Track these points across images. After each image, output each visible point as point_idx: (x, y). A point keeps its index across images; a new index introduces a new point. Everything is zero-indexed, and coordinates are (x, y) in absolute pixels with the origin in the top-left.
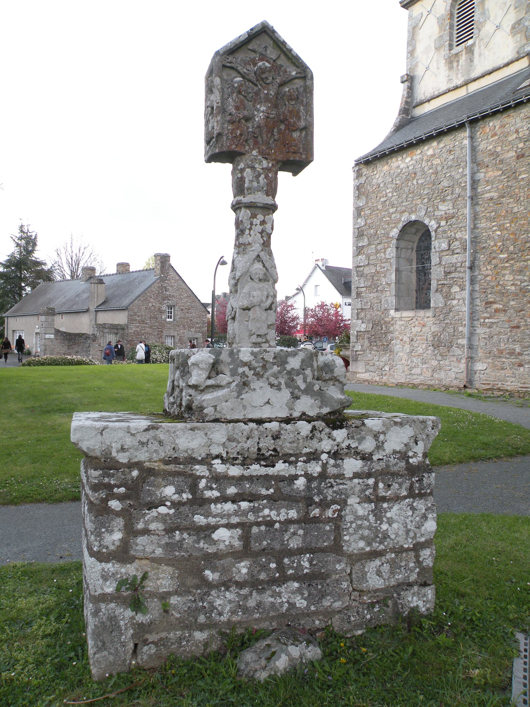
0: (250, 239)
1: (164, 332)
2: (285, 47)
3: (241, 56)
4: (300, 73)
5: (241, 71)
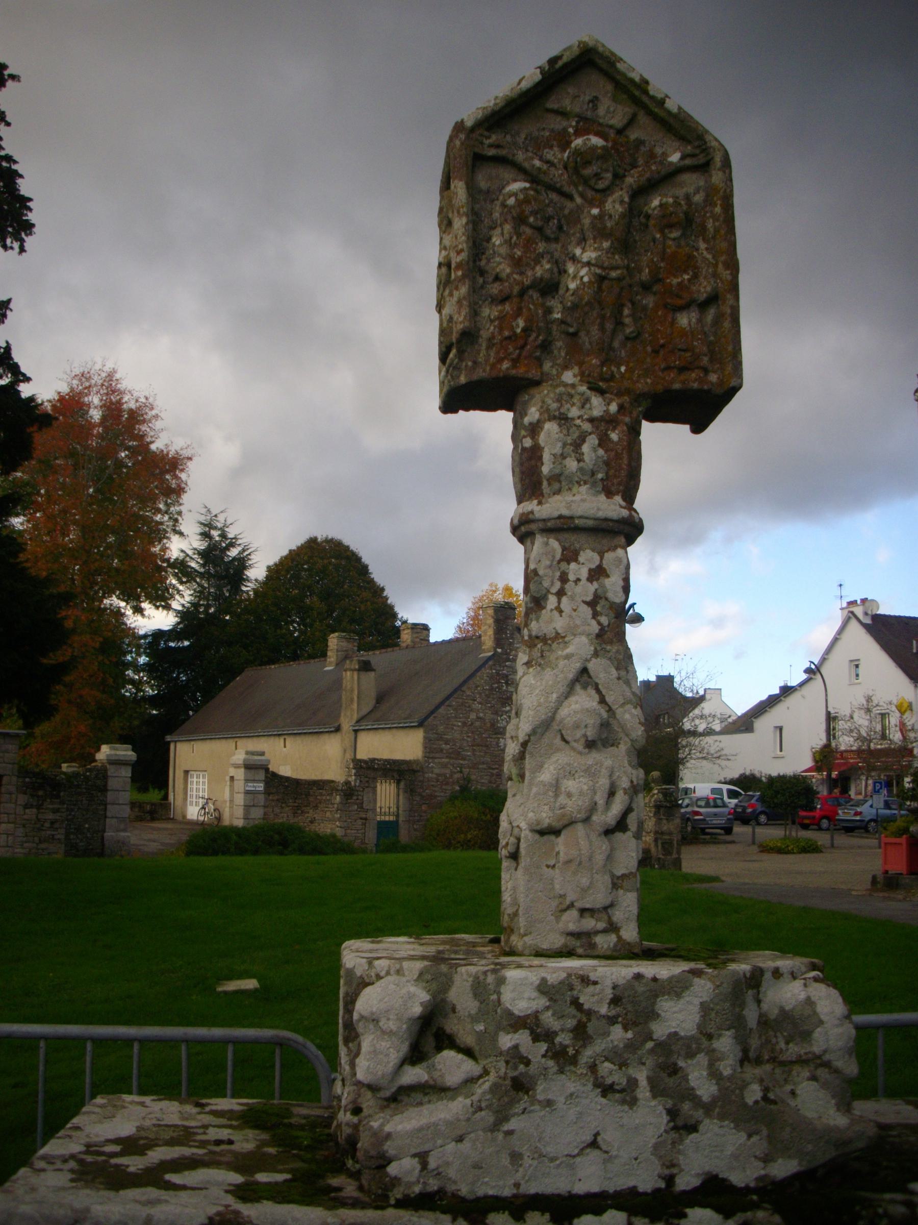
0: (560, 624)
2: (646, 92)
3: (526, 129)
4: (693, 156)
5: (526, 165)
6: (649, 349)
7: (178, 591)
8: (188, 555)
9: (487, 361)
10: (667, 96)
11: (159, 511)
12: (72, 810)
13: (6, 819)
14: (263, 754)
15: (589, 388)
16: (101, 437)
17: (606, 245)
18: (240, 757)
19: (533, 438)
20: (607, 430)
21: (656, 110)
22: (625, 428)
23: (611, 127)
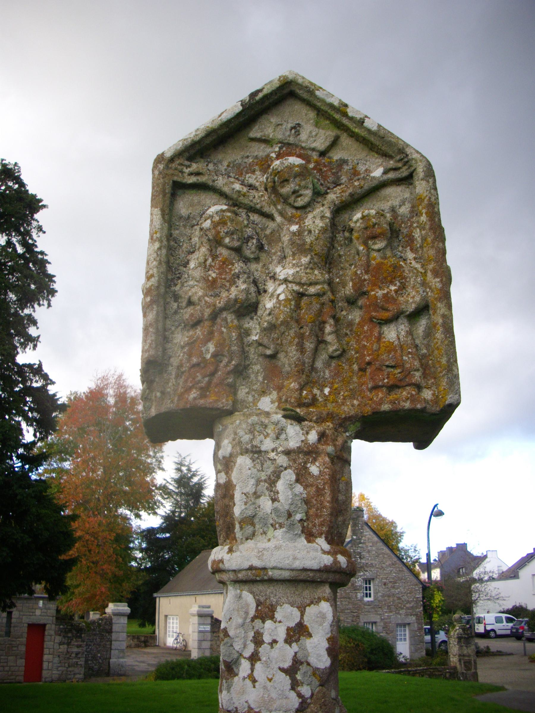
1: (361, 617)
4: (395, 169)
5: (226, 189)
6: (355, 367)
7: (162, 504)
8: (168, 482)
9: (175, 391)
10: (366, 117)
11: (149, 456)
12: (90, 645)
13: (48, 652)
14: (209, 607)
15: (285, 416)
16: (115, 413)
17: (305, 260)
18: (195, 609)
19: (227, 473)
20: (305, 463)
21: (357, 130)
22: (327, 459)
23: (313, 150)
